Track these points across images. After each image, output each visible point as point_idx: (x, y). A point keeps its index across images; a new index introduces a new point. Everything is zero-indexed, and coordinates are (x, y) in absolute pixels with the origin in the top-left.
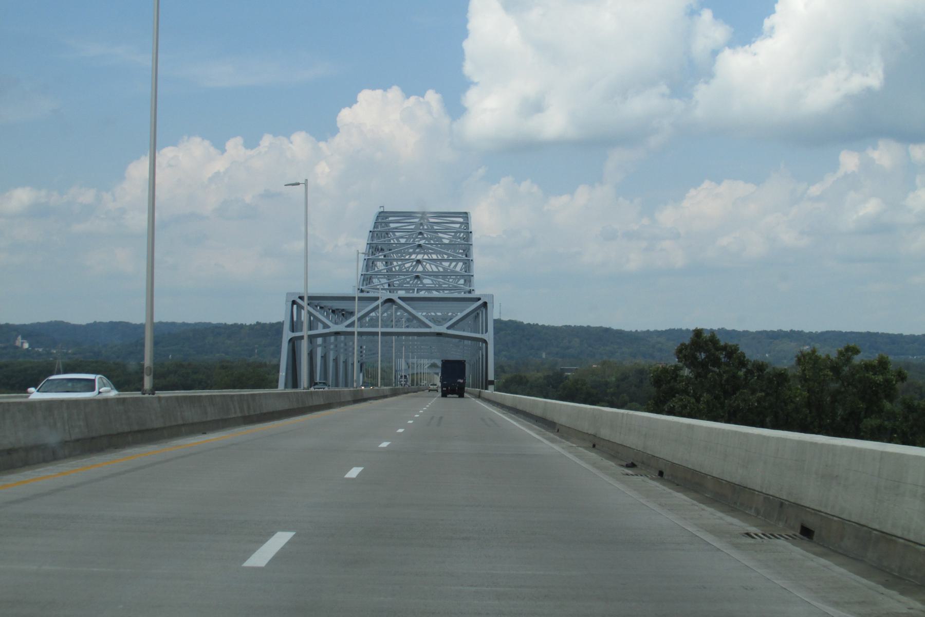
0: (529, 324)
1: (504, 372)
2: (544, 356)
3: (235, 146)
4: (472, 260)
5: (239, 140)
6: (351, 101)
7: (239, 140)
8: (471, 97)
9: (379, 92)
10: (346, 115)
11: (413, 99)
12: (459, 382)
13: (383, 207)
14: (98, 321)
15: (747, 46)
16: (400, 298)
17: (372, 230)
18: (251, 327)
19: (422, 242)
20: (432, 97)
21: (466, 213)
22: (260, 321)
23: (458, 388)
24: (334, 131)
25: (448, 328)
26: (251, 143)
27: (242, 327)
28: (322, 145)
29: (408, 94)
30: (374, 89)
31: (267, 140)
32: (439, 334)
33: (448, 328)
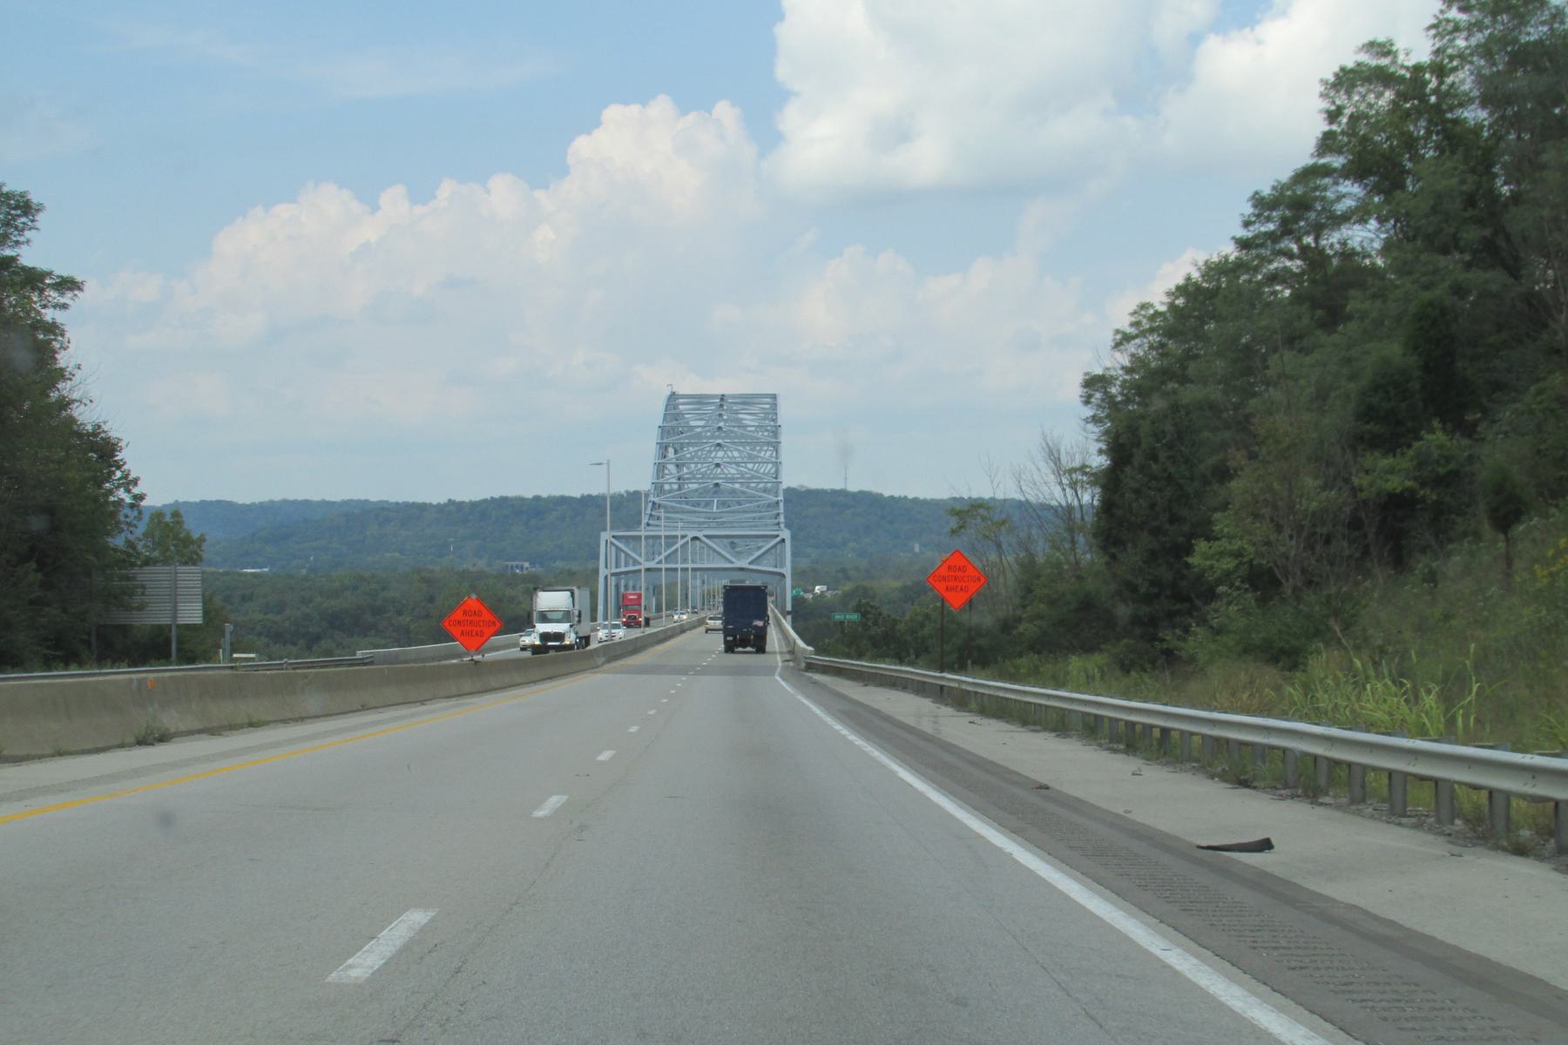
0: (892, 497)
1: (848, 578)
2: (917, 549)
3: (394, 201)
4: (780, 463)
5: (399, 190)
6: (592, 123)
7: (399, 190)
8: (791, 118)
9: (635, 109)
10: (582, 146)
11: (692, 117)
12: (756, 626)
13: (671, 385)
14: (181, 500)
15: (1247, 30)
16: (705, 536)
17: (662, 425)
18: (440, 508)
19: (721, 424)
20: (725, 111)
21: (775, 395)
22: (453, 499)
23: (755, 636)
24: (563, 171)
25: (750, 563)
26: (421, 194)
27: (423, 508)
28: (540, 194)
29: (684, 107)
30: (626, 103)
31: (447, 189)
32: (742, 569)
33: (750, 563)
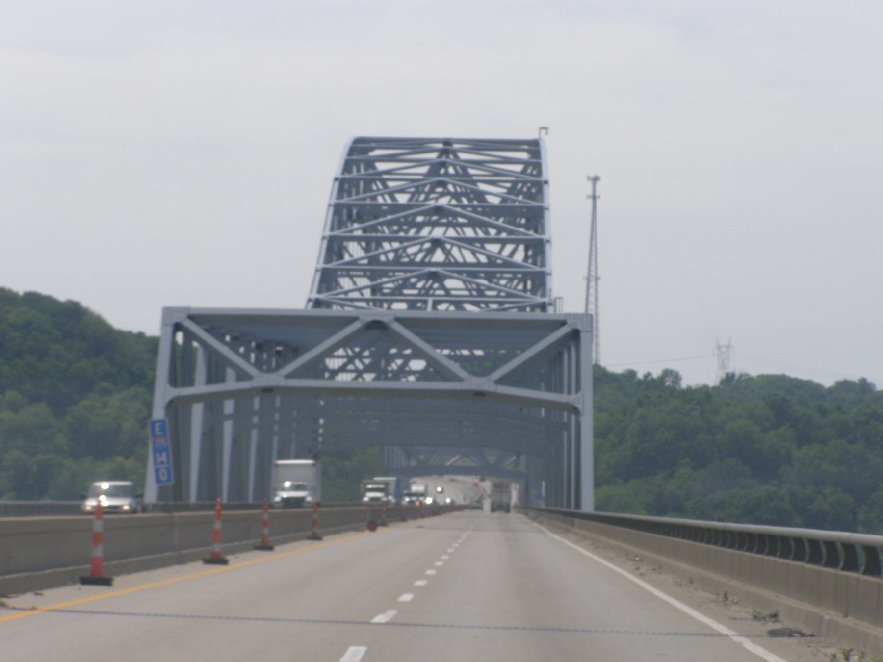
4: (548, 241)
25: (500, 382)
